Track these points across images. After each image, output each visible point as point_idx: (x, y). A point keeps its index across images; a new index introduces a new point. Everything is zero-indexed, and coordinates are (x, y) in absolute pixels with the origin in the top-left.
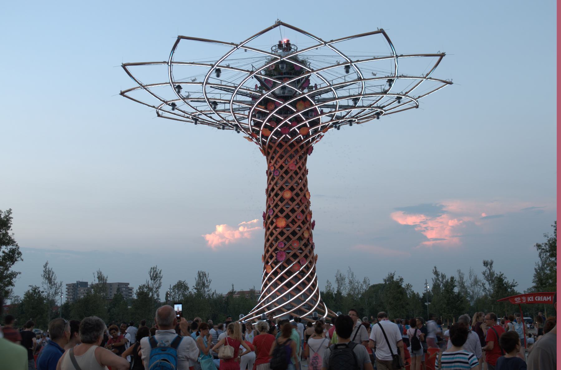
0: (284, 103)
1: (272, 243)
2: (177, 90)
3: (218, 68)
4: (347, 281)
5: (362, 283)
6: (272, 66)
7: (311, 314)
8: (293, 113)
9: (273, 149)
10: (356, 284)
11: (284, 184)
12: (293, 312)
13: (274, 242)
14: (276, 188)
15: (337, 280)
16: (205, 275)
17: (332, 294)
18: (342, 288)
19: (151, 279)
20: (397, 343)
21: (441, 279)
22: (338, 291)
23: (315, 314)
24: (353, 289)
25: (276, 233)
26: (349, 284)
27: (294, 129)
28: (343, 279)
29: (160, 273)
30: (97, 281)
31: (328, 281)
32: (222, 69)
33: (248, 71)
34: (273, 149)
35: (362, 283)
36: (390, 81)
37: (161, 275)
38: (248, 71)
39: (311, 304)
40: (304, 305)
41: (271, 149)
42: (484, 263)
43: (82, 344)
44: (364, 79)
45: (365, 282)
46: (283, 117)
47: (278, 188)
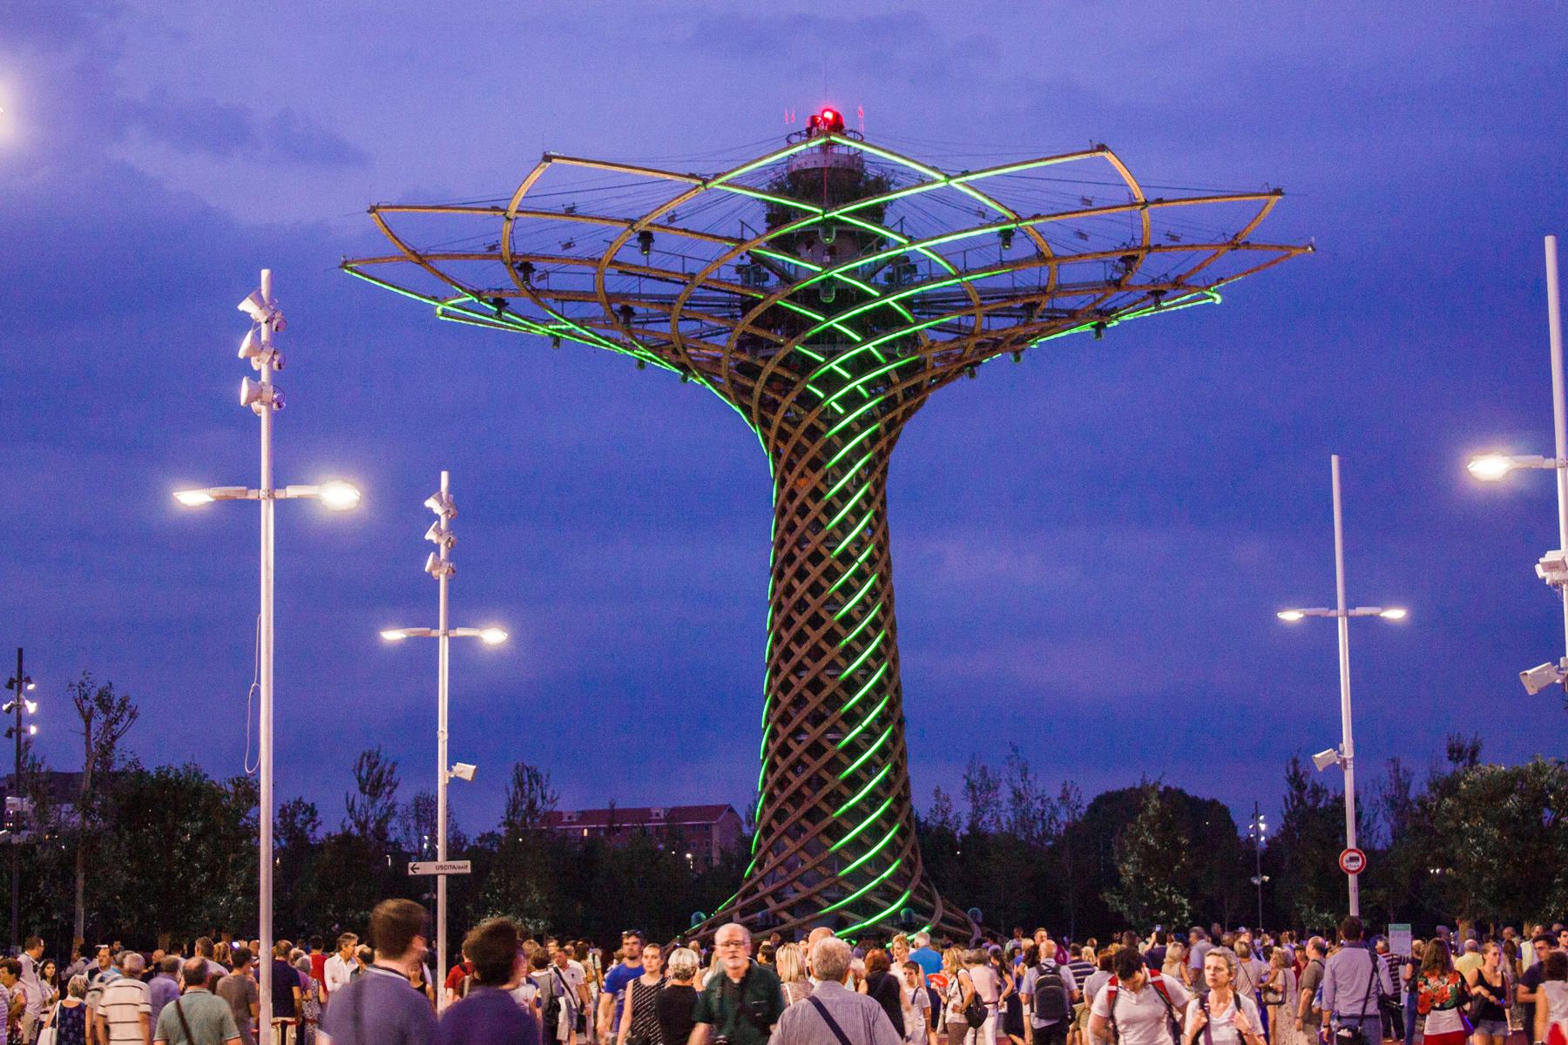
0: (828, 320)
1: (785, 712)
2: (521, 275)
3: (649, 229)
4: (1005, 793)
5: (1056, 803)
6: (777, 164)
7: (896, 914)
8: (851, 343)
9: (792, 443)
10: (1038, 804)
11: (823, 542)
12: (845, 908)
13: (792, 710)
14: (801, 557)
15: (971, 786)
16: (535, 777)
17: (953, 836)
18: (986, 818)
19: (362, 789)
20: (1139, 1002)
21: (1310, 802)
22: (972, 827)
23: (908, 915)
24: (1025, 822)
25: (798, 684)
26: (1011, 802)
27: (855, 390)
28: (991, 787)
29: (391, 772)
30: (339, 832)
31: (937, 792)
32: (655, 230)
33: (730, 239)
34: (792, 443)
35: (1056, 803)
36: (1129, 261)
37: (395, 777)
38: (730, 239)
39: (897, 887)
40: (876, 889)
41: (786, 442)
42: (1451, 751)
43: (746, 965)
44: (1055, 257)
45: (1064, 798)
46: (822, 354)
47: (807, 554)
